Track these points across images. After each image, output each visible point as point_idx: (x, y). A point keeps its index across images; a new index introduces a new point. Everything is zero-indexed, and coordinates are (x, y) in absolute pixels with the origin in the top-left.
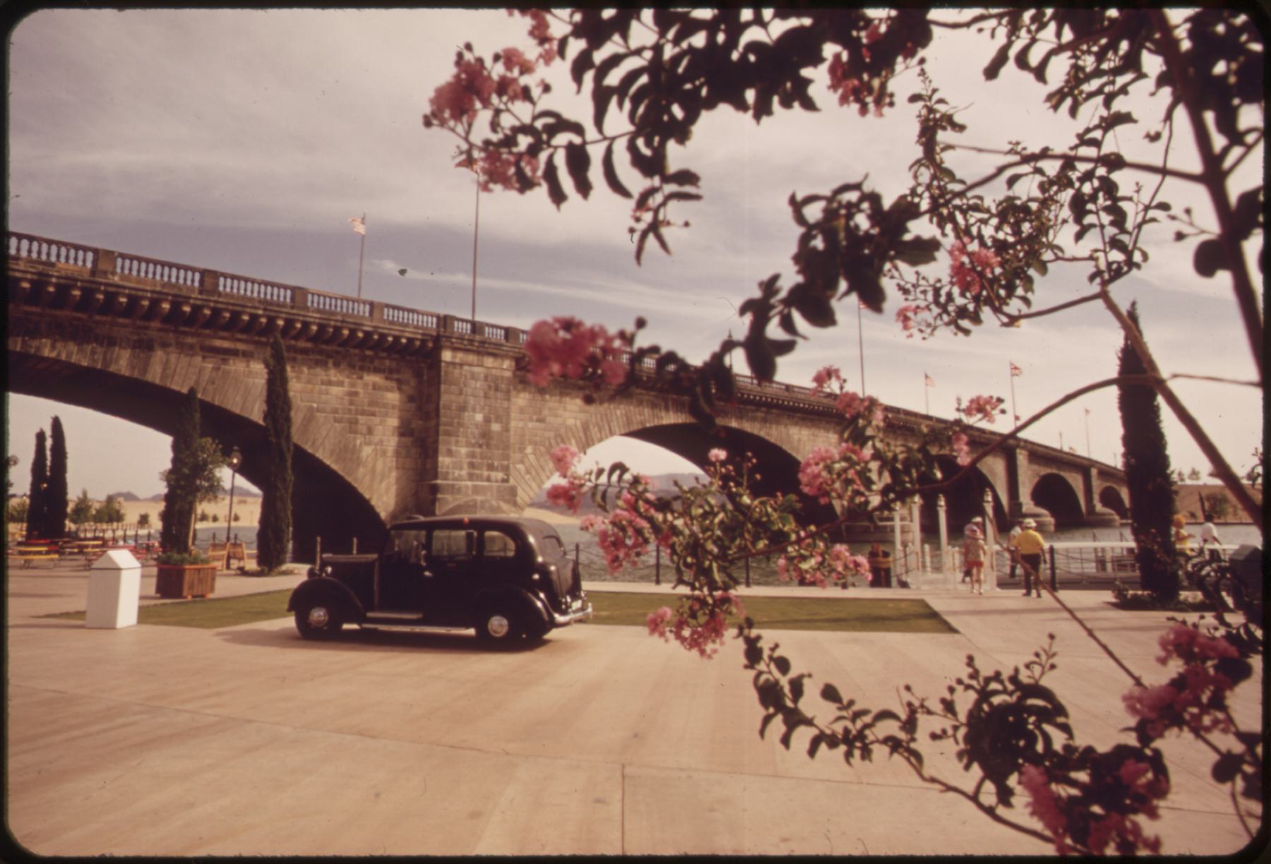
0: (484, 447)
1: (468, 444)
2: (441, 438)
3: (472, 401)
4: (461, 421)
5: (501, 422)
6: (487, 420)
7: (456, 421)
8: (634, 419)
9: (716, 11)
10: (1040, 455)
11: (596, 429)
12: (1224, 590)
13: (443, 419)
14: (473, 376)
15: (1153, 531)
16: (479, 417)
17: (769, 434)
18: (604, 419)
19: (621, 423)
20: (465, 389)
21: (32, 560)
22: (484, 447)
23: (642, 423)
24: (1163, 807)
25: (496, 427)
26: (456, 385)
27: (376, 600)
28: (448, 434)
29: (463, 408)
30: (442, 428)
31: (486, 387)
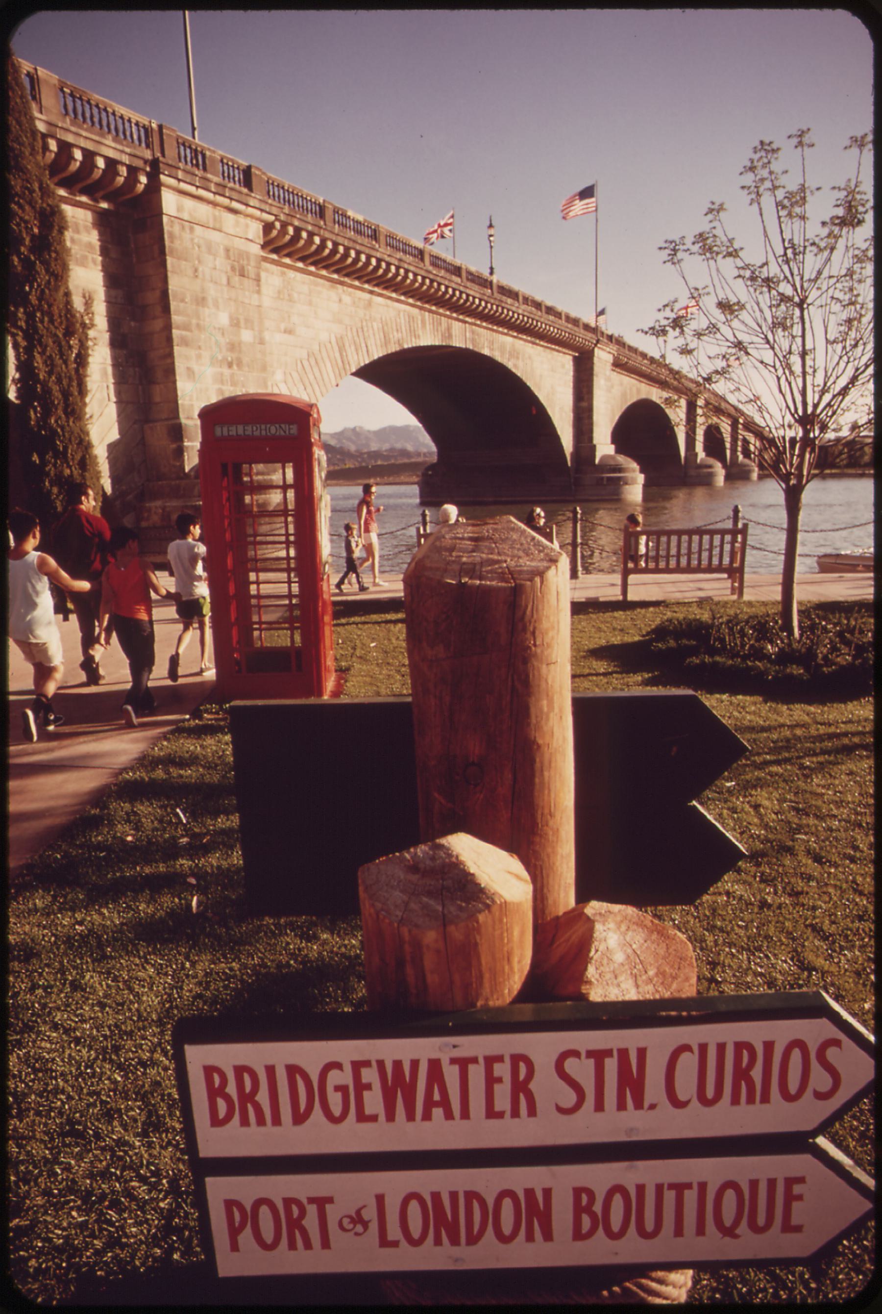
0: (235, 367)
1: (214, 361)
2: (177, 350)
3: (212, 292)
4: (201, 322)
5: (253, 329)
6: (235, 323)
7: (194, 321)
8: (391, 336)
9: (873, 1188)
10: (718, 408)
11: (353, 348)
12: (201, 841)
13: (176, 318)
14: (210, 248)
15: (175, 1238)
16: (223, 319)
17: (515, 366)
18: (360, 334)
19: (378, 342)
20: (200, 269)
21: (646, 683)
22: (235, 367)
23: (399, 342)
24: (169, 187)
25: (246, 336)
26: (186, 260)
27: (35, 738)
28: (185, 342)
29: (201, 301)
30: (175, 332)
31: (229, 268)
